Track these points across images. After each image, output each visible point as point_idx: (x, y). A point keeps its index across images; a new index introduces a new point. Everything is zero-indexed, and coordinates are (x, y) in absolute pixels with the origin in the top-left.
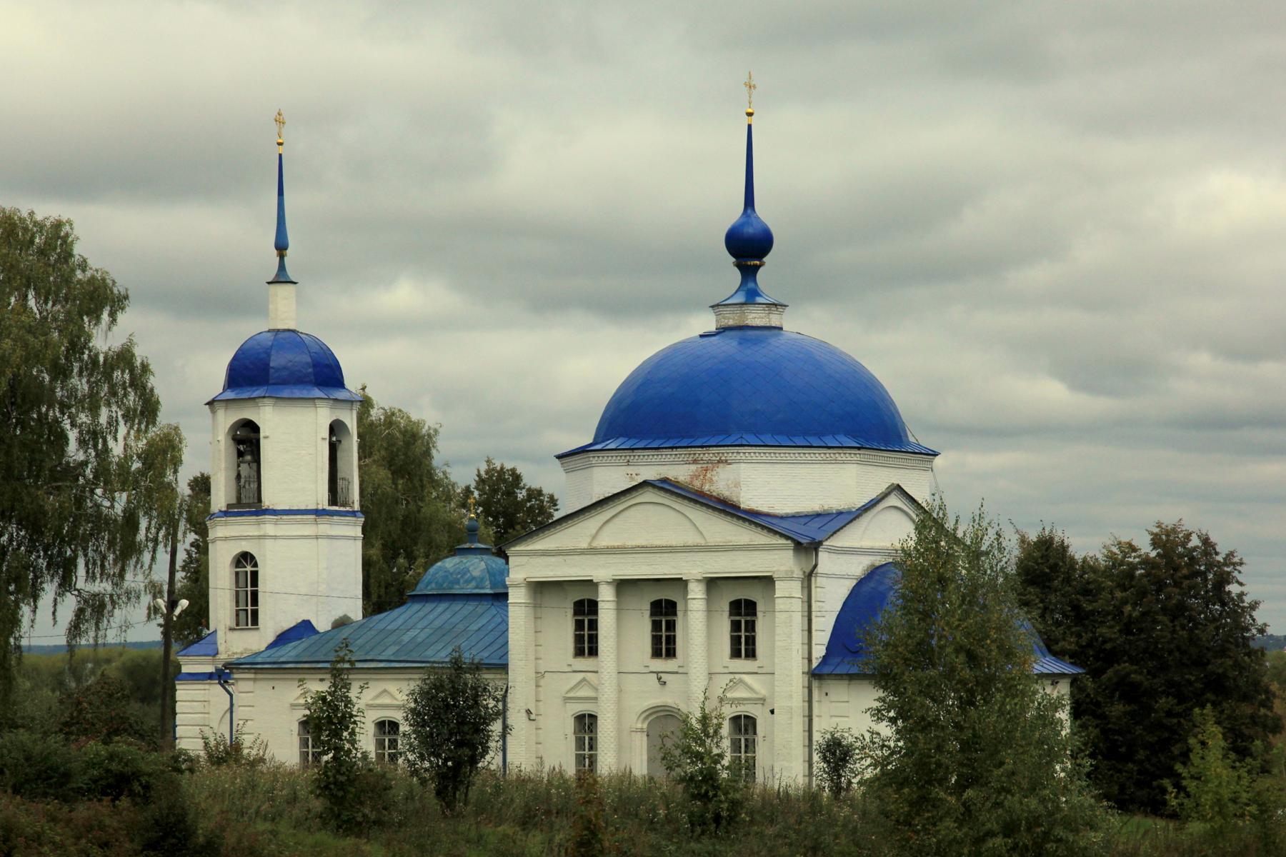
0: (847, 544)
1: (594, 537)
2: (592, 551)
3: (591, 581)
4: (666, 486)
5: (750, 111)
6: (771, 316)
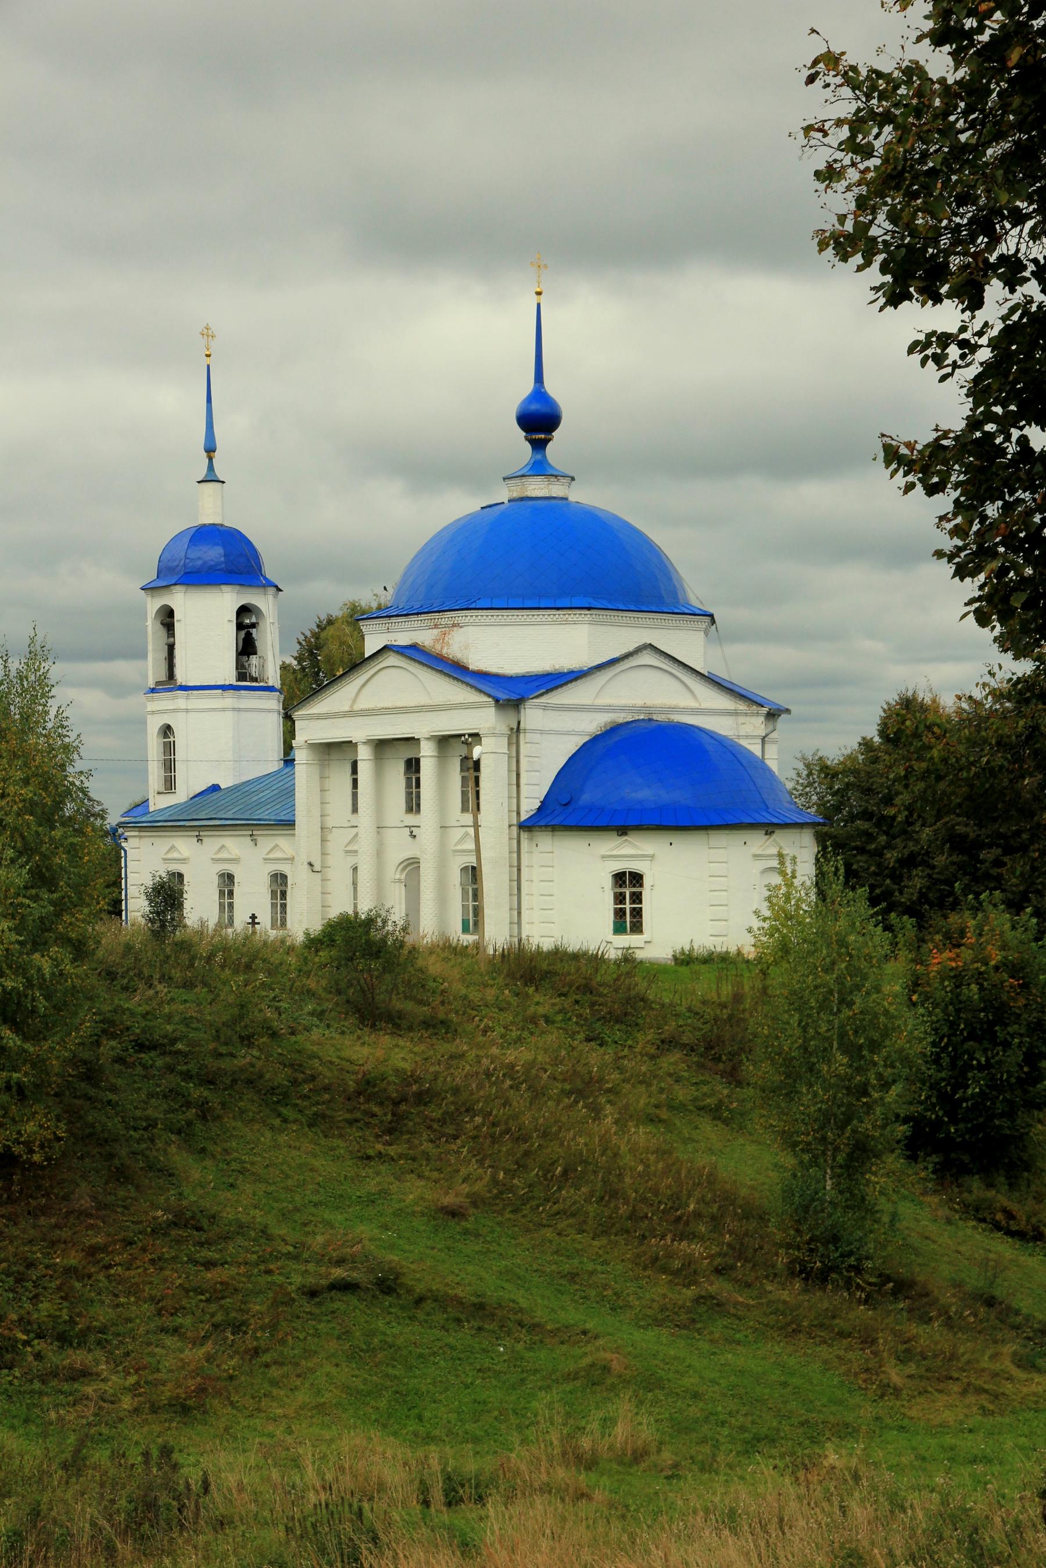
0: (571, 702)
1: (354, 701)
2: (351, 714)
3: (351, 742)
4: (414, 653)
5: (538, 290)
6: (551, 487)
